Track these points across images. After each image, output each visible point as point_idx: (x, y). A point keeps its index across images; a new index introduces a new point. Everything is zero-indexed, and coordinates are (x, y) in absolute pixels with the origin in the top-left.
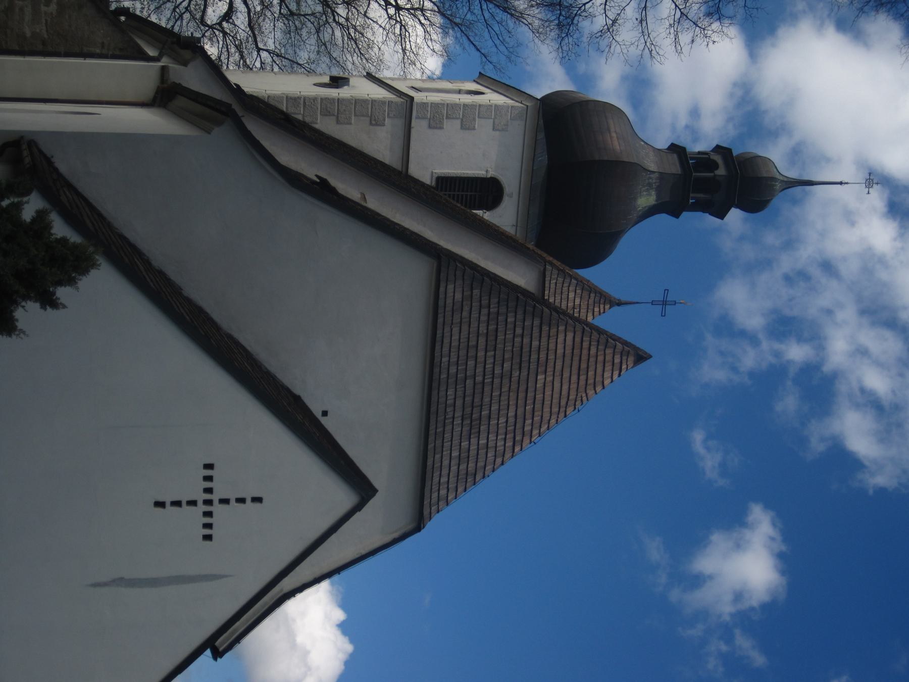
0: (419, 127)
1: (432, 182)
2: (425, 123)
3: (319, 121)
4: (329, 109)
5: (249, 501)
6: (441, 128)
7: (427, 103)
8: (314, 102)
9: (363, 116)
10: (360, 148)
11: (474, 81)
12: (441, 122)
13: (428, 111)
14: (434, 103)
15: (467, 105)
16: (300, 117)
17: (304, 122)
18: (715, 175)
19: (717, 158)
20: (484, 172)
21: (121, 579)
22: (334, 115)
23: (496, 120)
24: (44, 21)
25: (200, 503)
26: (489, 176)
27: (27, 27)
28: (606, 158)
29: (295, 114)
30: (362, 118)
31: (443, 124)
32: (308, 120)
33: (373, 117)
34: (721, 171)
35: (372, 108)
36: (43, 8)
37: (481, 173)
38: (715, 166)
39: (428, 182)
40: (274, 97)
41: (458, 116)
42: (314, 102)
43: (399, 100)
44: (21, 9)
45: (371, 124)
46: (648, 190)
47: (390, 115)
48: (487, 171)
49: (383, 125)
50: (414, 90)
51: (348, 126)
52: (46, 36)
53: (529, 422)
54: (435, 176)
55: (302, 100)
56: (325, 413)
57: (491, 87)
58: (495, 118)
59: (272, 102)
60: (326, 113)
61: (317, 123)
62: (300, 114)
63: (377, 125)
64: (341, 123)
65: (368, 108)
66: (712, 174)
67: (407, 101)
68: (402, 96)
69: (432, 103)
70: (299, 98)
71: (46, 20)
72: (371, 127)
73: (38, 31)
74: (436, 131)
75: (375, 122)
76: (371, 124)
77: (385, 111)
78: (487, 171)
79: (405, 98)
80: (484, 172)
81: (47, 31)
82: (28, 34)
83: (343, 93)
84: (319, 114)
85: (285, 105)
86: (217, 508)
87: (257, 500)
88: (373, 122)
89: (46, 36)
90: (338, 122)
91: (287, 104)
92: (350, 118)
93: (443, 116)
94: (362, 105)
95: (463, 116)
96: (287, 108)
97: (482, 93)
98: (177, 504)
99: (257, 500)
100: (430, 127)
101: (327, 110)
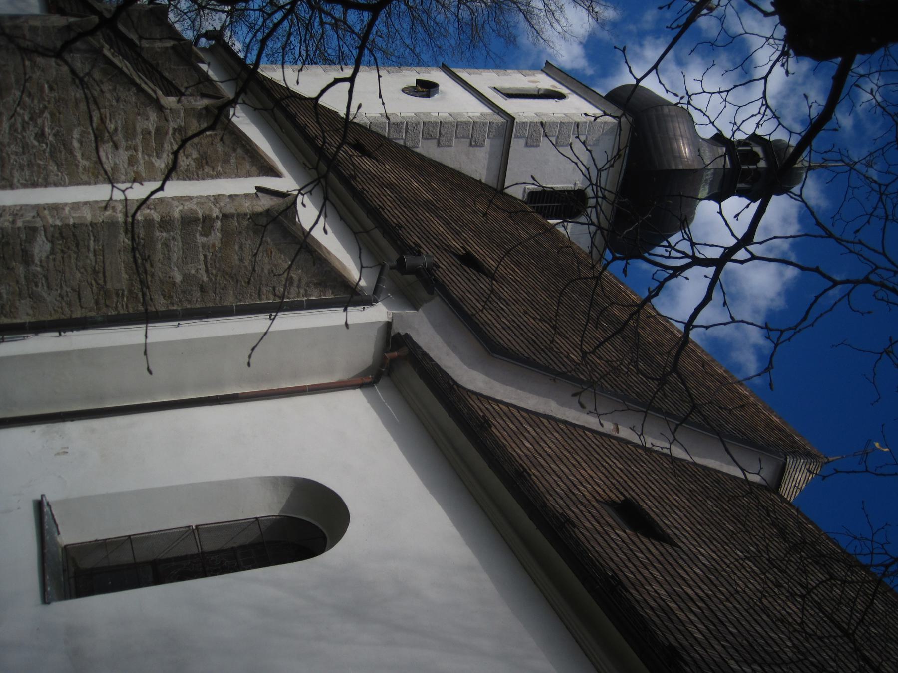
0: (517, 145)
1: (523, 197)
2: (522, 142)
3: (420, 145)
4: (431, 132)
6: (537, 146)
7: (527, 122)
8: (416, 125)
9: (464, 137)
10: (458, 170)
11: (542, 70)
12: (538, 141)
13: (526, 130)
14: (533, 122)
15: (564, 123)
16: (401, 142)
17: (405, 147)
19: (758, 149)
20: (572, 186)
22: (435, 138)
23: (589, 136)
24: (202, 257)
26: (576, 189)
27: (176, 269)
28: (681, 167)
29: (396, 139)
30: (463, 139)
31: (539, 142)
32: (409, 144)
33: (474, 139)
34: (762, 164)
35: (473, 128)
36: (200, 239)
37: (569, 186)
39: (520, 197)
40: (377, 123)
41: (554, 134)
42: (416, 125)
43: (499, 119)
44: (166, 245)
45: (471, 145)
47: (490, 136)
48: (575, 184)
49: (483, 145)
50: (500, 94)
51: (448, 148)
52: (205, 279)
54: (528, 191)
55: (404, 125)
56: (364, 308)
57: (566, 84)
58: (588, 134)
59: (374, 129)
60: (427, 136)
61: (417, 147)
62: (402, 138)
63: (476, 146)
64: (442, 146)
65: (469, 130)
66: (755, 167)
67: (507, 121)
68: (500, 113)
69: (531, 122)
70: (402, 123)
71: (205, 256)
72: (471, 148)
73: (193, 272)
74: (533, 148)
75: (474, 143)
76: (471, 145)
77: (486, 132)
78: (575, 184)
79: (506, 118)
80: (572, 186)
81: (207, 271)
82: (178, 278)
83: (410, 77)
84: (421, 138)
85: (387, 131)
88: (473, 143)
89: (205, 279)
90: (439, 145)
91: (389, 129)
92: (451, 140)
93: (540, 134)
94: (463, 127)
95: (559, 134)
96: (389, 133)
97: (560, 96)
100: (527, 145)
101: (428, 134)
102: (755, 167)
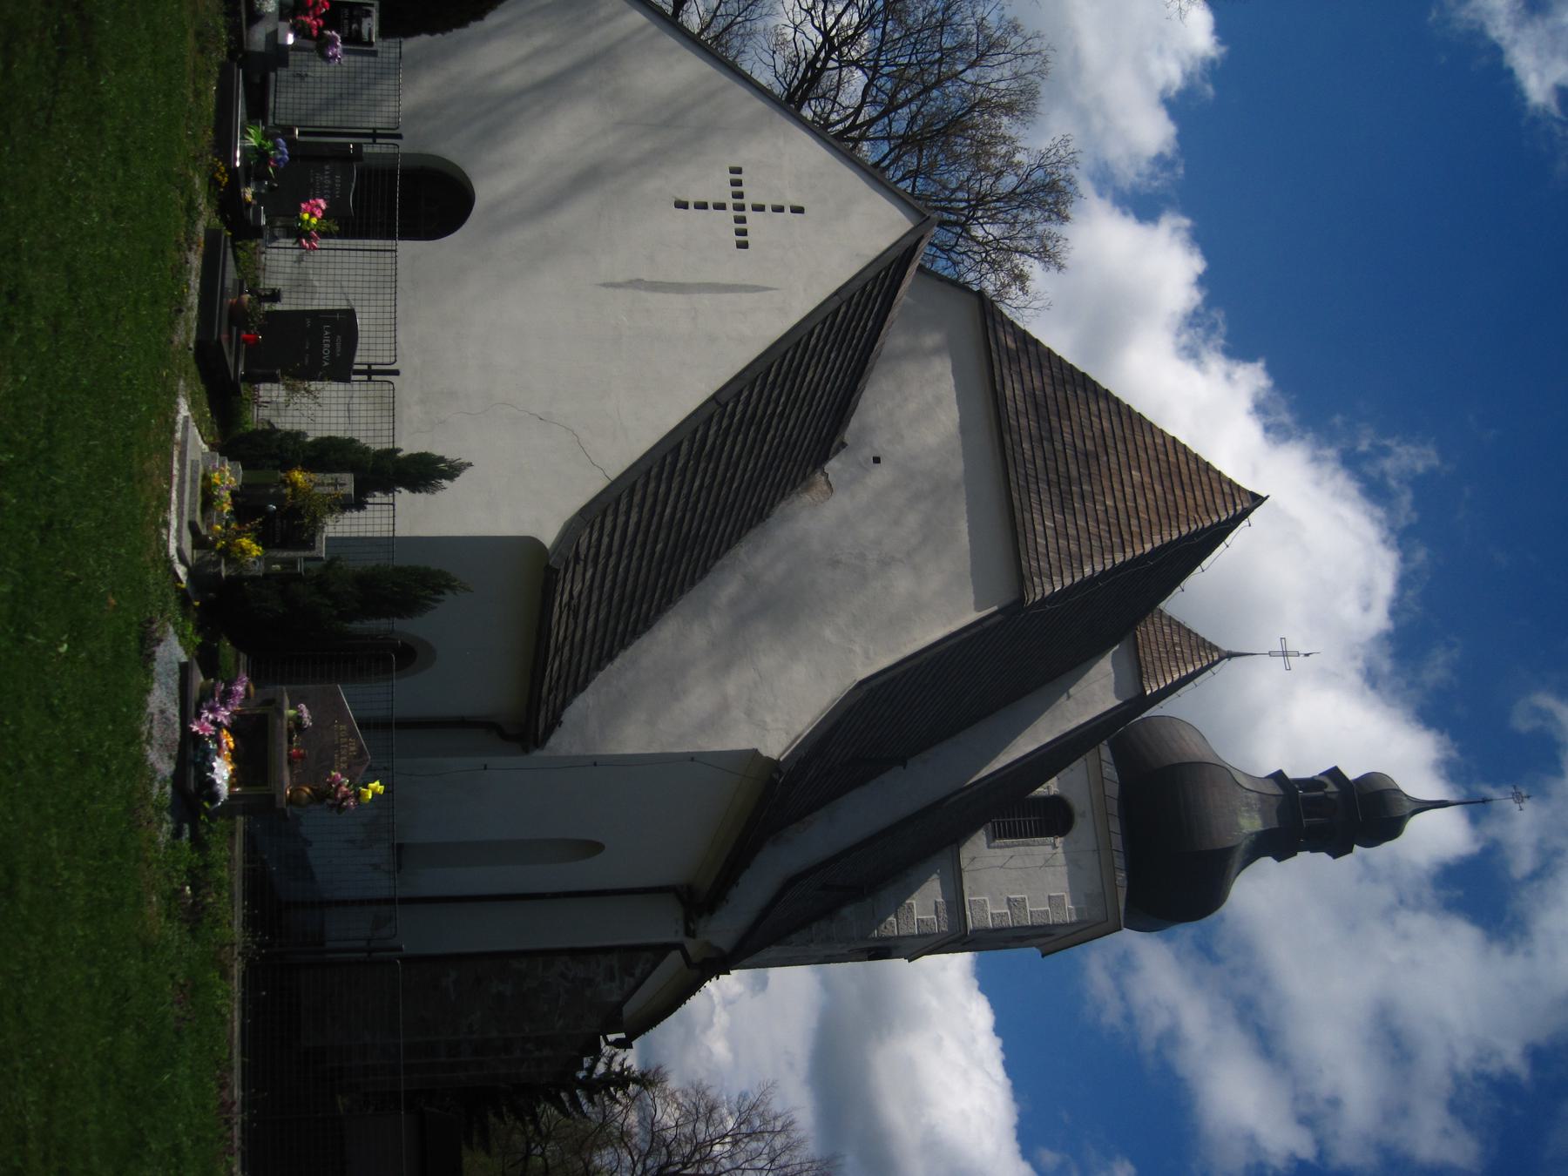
5: (787, 210)
18: (1326, 793)
21: (639, 281)
25: (730, 207)
26: (1052, 793)
38: (1326, 786)
46: (1248, 811)
53: (1134, 522)
66: (1321, 793)
86: (749, 213)
87: (798, 210)
98: (702, 206)
99: (798, 210)
102: (1321, 793)
